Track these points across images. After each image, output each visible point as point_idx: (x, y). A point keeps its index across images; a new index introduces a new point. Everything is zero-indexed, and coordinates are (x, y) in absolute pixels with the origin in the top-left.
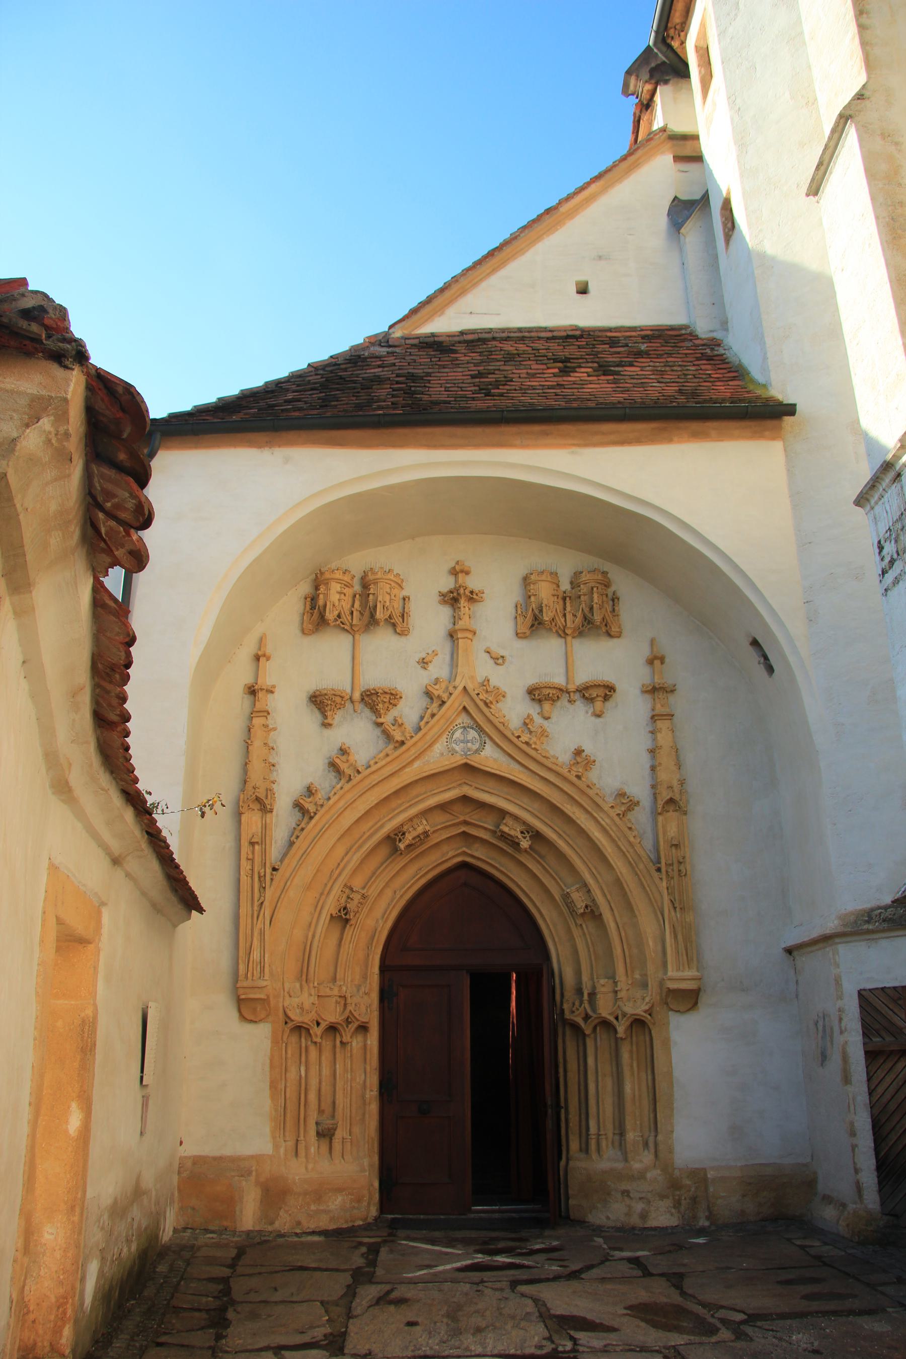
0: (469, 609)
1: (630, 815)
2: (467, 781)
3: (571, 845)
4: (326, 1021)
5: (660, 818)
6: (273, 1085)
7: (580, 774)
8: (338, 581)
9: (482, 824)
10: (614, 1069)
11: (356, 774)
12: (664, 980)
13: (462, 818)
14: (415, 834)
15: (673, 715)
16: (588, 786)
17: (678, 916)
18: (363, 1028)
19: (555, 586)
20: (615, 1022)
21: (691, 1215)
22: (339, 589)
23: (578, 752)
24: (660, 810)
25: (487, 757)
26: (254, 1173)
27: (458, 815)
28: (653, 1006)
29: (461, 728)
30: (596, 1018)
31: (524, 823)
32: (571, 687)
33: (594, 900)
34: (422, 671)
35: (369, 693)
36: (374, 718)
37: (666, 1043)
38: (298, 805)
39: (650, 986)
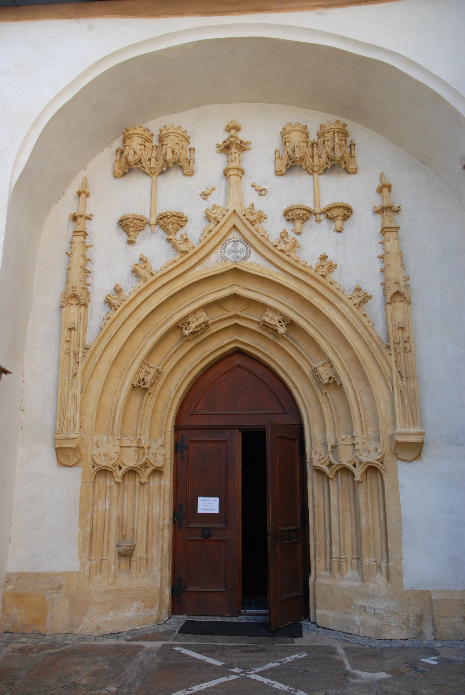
0: (239, 155)
1: (365, 306)
2: (237, 283)
3: (317, 330)
4: (126, 466)
5: (389, 307)
6: (82, 514)
7: (324, 273)
8: (140, 136)
9: (249, 317)
10: (353, 506)
11: (150, 276)
12: (393, 434)
13: (234, 313)
14: (197, 323)
15: (398, 228)
16: (331, 283)
17: (405, 383)
18: (158, 471)
19: (305, 136)
20: (353, 468)
21: (418, 630)
22: (140, 142)
23: (324, 258)
24: (389, 300)
25: (252, 263)
26: (64, 587)
27: (232, 311)
28: (384, 456)
29: (232, 241)
30: (338, 465)
31: (281, 314)
32: (317, 210)
33: (336, 373)
34: (203, 201)
35: (161, 217)
36: (166, 236)
37: (396, 486)
38: (108, 302)
39: (381, 439)
